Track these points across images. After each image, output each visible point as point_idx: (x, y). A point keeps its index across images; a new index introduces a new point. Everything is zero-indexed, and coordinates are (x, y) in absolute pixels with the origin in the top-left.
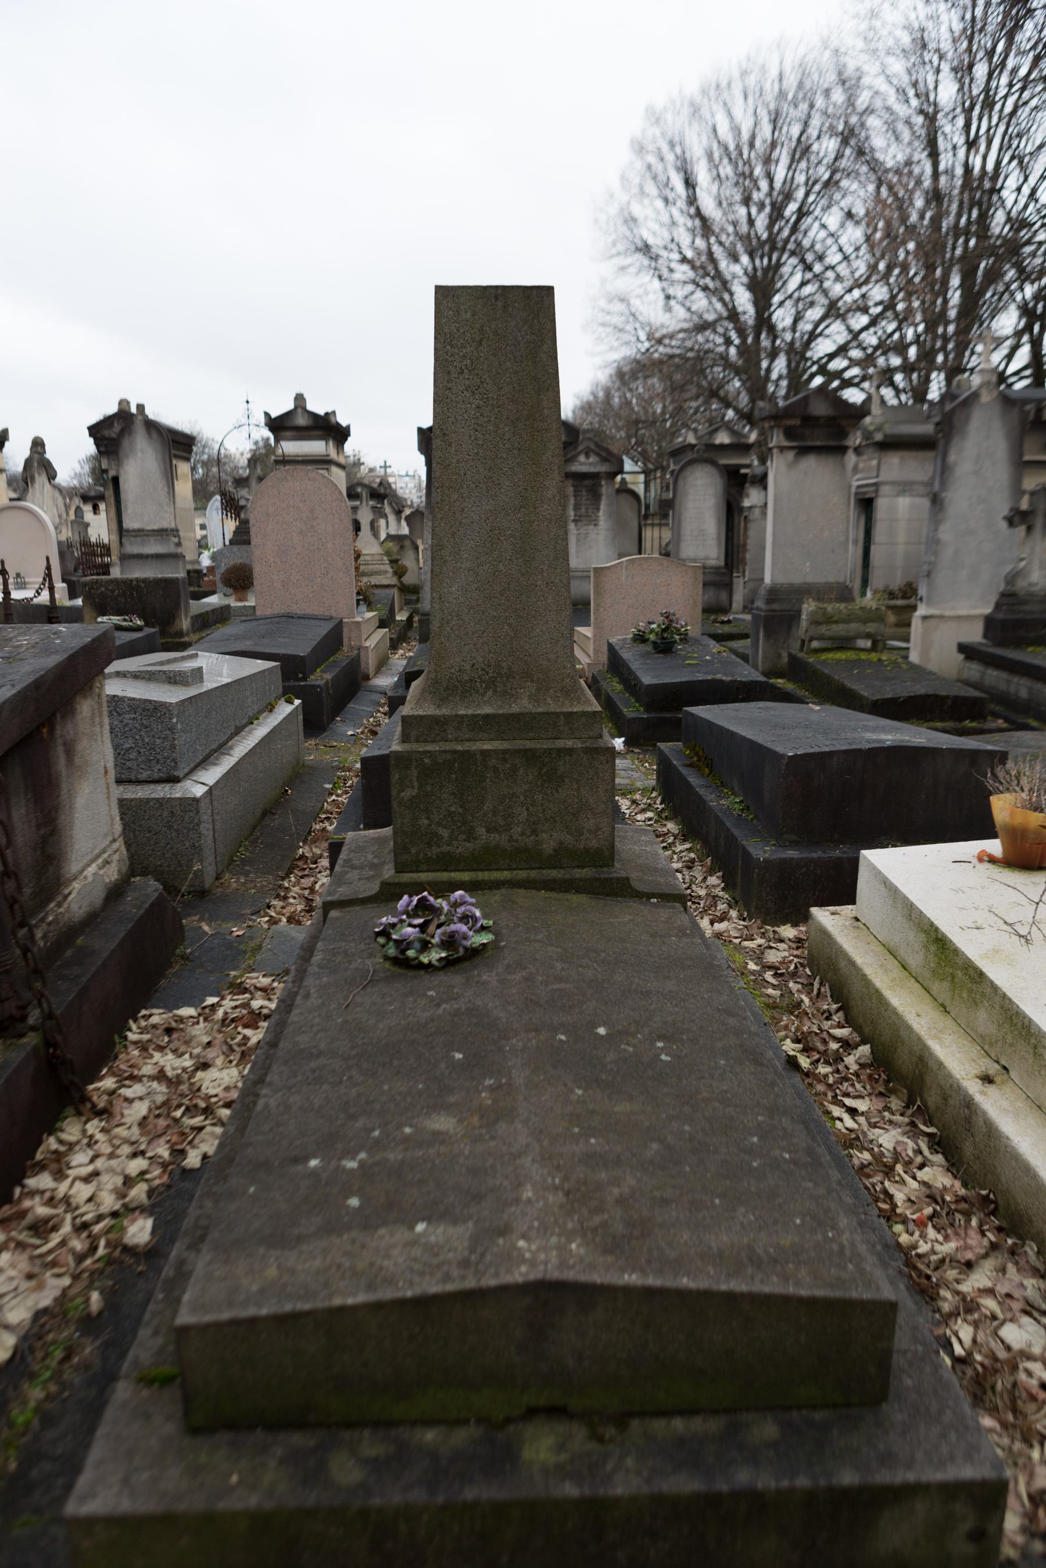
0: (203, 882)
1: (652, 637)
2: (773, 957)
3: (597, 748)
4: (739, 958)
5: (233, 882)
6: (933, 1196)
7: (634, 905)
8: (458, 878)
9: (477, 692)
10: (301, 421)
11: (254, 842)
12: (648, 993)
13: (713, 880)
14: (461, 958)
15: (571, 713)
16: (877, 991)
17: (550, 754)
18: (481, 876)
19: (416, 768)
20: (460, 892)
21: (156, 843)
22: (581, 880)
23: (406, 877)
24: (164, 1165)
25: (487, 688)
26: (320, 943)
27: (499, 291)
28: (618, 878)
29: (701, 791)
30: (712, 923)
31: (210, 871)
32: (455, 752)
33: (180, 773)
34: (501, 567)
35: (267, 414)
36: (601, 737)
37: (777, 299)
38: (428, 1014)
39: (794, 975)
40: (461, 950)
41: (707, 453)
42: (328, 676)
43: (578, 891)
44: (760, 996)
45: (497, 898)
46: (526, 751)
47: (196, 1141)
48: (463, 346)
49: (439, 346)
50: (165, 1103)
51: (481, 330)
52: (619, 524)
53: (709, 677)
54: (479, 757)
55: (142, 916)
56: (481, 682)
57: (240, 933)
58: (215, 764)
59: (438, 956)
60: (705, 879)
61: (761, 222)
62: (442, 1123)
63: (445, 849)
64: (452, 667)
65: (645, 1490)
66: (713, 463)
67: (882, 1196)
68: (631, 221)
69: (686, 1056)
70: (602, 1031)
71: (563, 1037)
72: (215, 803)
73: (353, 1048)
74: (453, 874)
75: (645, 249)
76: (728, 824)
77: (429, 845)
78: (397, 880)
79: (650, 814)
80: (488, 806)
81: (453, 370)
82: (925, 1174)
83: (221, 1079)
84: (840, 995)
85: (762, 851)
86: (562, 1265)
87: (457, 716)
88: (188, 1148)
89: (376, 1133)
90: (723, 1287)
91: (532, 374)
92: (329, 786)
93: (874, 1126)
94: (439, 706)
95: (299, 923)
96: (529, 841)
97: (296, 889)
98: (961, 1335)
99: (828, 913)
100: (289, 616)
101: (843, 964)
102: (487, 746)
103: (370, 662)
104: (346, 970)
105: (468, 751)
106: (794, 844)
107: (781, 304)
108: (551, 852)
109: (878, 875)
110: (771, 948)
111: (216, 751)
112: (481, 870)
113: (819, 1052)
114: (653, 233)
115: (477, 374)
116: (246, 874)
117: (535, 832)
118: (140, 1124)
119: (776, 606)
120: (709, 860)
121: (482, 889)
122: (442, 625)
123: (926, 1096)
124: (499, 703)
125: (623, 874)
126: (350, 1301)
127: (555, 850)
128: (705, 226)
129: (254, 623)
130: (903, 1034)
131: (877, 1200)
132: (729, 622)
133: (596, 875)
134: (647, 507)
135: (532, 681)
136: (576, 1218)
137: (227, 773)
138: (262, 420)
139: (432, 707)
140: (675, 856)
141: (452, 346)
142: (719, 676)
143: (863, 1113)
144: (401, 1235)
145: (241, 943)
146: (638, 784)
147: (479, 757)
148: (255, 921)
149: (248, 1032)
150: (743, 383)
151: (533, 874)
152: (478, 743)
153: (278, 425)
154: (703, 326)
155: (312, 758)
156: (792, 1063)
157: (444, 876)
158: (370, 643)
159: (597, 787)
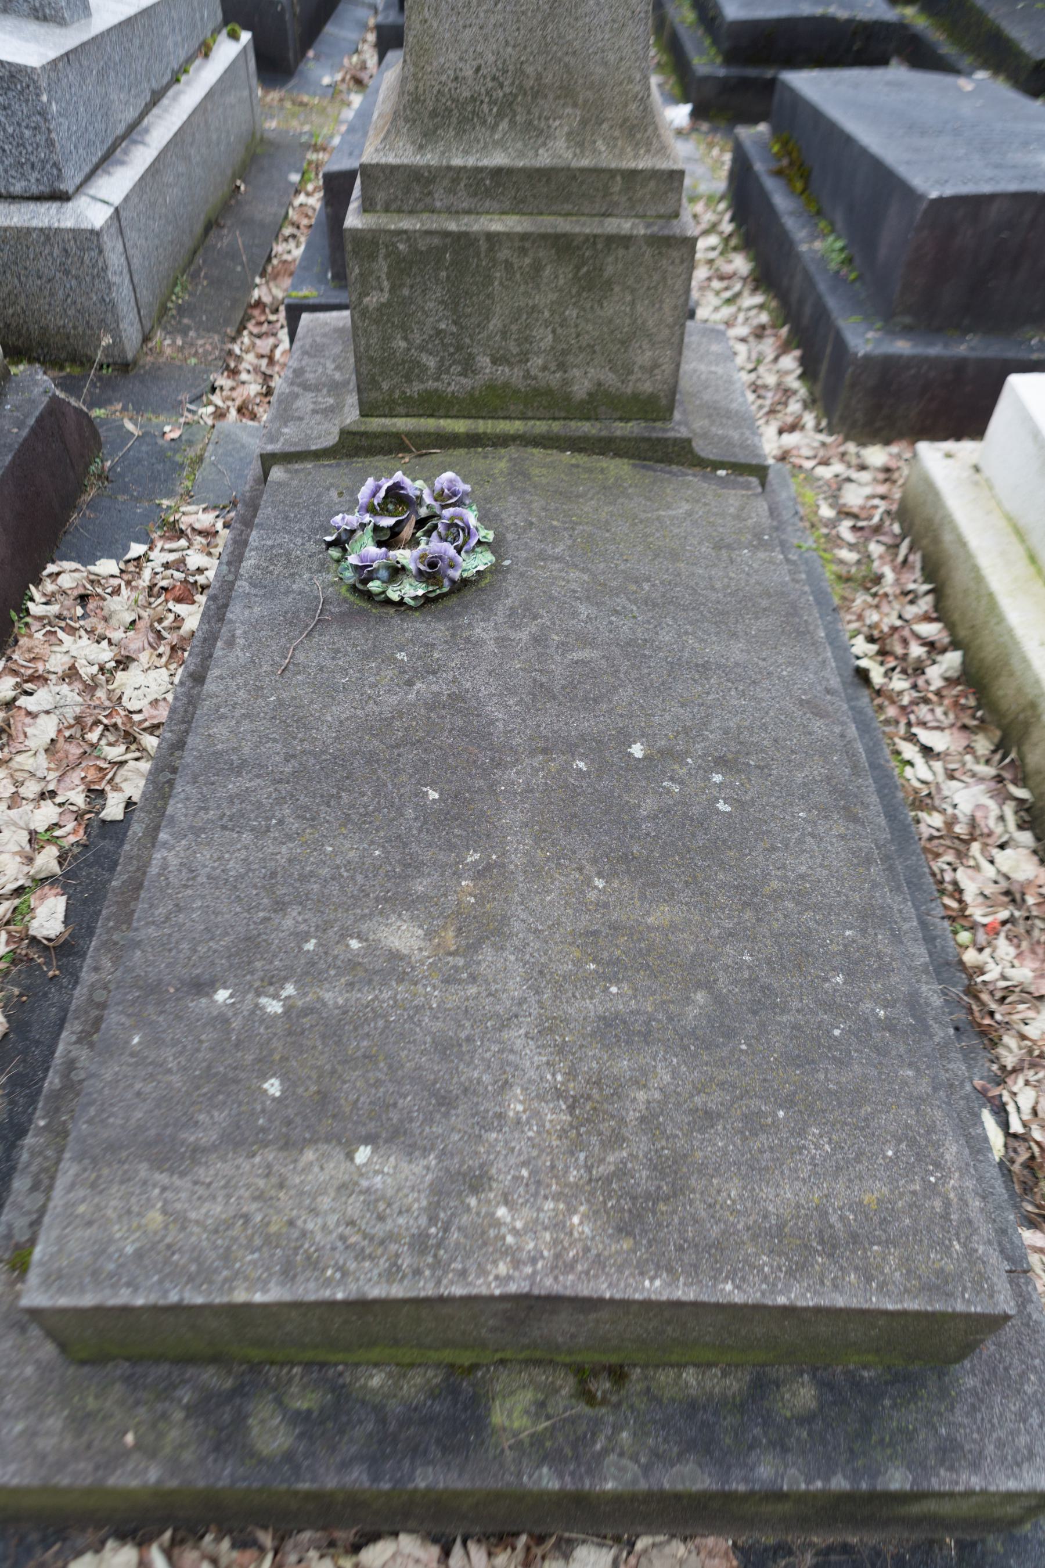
0: (123, 351)
2: (853, 497)
4: (809, 495)
5: (166, 344)
6: (1012, 896)
7: (693, 478)
8: (449, 429)
11: (195, 276)
12: (704, 668)
14: (447, 593)
16: (991, 595)
17: (595, 243)
18: (483, 426)
20: (449, 475)
21: (52, 295)
22: (623, 439)
23: (376, 424)
24: (79, 816)
25: (500, 116)
26: (254, 533)
28: (675, 440)
29: (790, 223)
30: (781, 432)
31: (131, 332)
32: (447, 234)
33: (68, 186)
36: (676, 215)
38: (394, 700)
39: (877, 530)
40: (446, 582)
43: (617, 454)
44: (832, 561)
45: (503, 465)
47: (117, 780)
50: (78, 719)
54: (483, 245)
55: (26, 440)
56: (490, 103)
57: (175, 435)
58: (122, 163)
59: (413, 593)
60: (776, 359)
62: (403, 936)
63: (431, 385)
64: (442, 70)
65: (643, 1485)
67: (950, 888)
69: (753, 800)
70: (637, 750)
71: (581, 765)
72: (127, 232)
73: (288, 758)
74: (442, 422)
76: (822, 287)
78: (363, 428)
80: (495, 323)
82: (1006, 859)
83: (148, 686)
84: (935, 572)
85: (864, 339)
86: (560, 1265)
87: (449, 168)
88: (108, 788)
89: (310, 946)
90: (781, 1300)
93: (951, 776)
94: (421, 147)
95: (254, 417)
96: (555, 379)
97: (250, 357)
98: (1020, 1099)
99: (939, 455)
101: (947, 538)
102: (497, 225)
104: (287, 593)
105: (466, 234)
106: (907, 331)
108: (585, 396)
109: (1026, 419)
110: (849, 480)
111: (123, 138)
112: (483, 418)
113: (896, 658)
116: (184, 331)
117: (562, 366)
118: (46, 751)
120: (784, 331)
121: (484, 446)
123: (1026, 748)
124: (519, 145)
125: (683, 432)
126: (258, 1298)
130: (1015, 661)
131: (942, 892)
133: (645, 432)
135: (575, 105)
136: (582, 1156)
137: (142, 178)
139: (410, 149)
143: (938, 754)
144: (335, 1169)
145: (176, 451)
147: (483, 245)
148: (194, 412)
149: (181, 609)
151: (556, 427)
156: (863, 676)
157: (429, 424)
159: (661, 302)
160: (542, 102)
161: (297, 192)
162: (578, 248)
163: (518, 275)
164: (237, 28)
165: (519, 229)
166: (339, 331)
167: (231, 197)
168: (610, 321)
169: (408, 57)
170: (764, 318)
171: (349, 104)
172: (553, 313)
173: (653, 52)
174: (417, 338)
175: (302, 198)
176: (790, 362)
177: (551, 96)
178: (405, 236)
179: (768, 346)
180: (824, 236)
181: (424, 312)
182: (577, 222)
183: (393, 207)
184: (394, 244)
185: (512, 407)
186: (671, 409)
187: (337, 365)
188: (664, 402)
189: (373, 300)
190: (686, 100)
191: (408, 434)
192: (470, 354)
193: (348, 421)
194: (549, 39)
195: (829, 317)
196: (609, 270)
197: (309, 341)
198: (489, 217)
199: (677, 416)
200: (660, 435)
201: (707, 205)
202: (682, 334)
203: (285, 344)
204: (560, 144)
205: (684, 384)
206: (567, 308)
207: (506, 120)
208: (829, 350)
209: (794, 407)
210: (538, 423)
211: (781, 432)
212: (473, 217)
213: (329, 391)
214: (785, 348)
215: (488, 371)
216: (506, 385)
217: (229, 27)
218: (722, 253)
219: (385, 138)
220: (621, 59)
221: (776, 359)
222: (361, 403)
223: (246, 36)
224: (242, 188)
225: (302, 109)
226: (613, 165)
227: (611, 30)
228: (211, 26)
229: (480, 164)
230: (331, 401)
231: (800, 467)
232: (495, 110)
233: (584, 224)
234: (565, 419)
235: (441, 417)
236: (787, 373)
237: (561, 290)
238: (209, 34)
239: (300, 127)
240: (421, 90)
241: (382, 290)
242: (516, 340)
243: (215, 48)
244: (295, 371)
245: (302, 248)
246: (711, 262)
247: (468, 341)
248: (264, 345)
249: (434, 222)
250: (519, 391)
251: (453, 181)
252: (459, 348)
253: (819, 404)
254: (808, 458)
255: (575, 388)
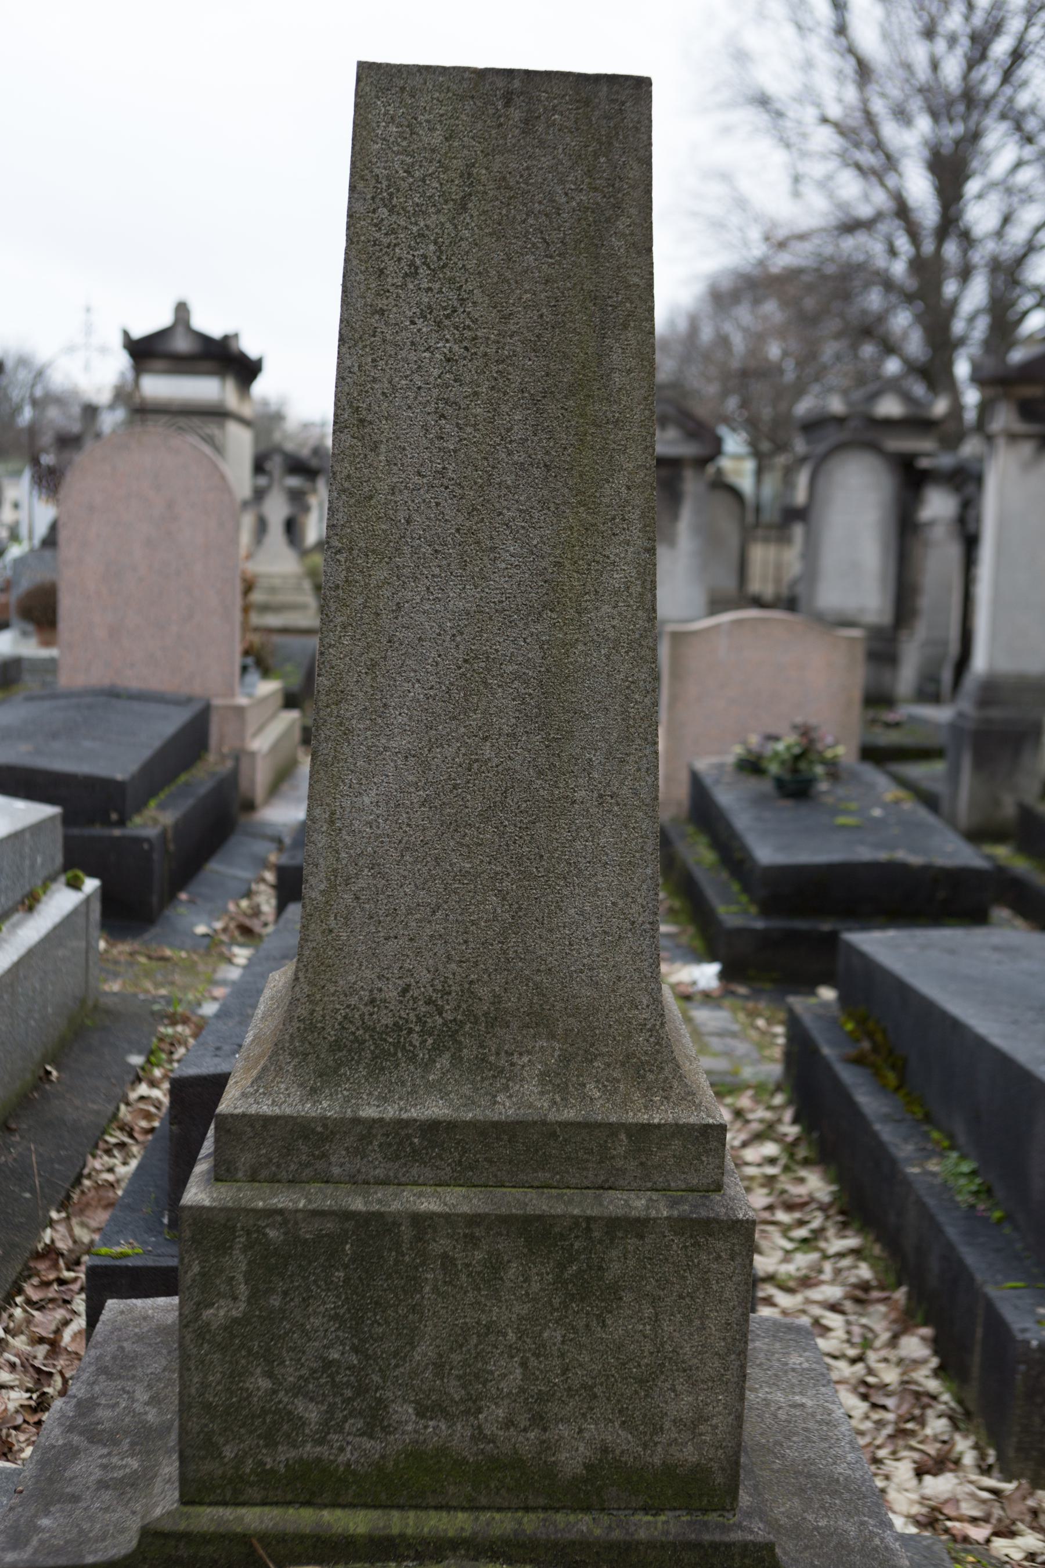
1: (774, 768)
3: (707, 1222)
8: (338, 1528)
9: (412, 1059)
10: (182, 344)
13: (914, 1345)
15: (647, 1128)
17: (588, 1229)
19: (244, 1250)
22: (651, 1545)
25: (438, 1049)
27: (517, 84)
28: (745, 1545)
29: (886, 1132)
30: (920, 1473)
32: (348, 1215)
34: (487, 751)
35: (126, 334)
36: (719, 1187)
37: (972, 187)
41: (863, 432)
42: (168, 818)
46: (527, 1220)
48: (420, 211)
49: (360, 207)
51: (467, 175)
52: (709, 539)
53: (883, 856)
54: (406, 1232)
61: (952, 70)
63: (310, 1450)
64: (353, 991)
66: (873, 447)
68: (741, 57)
74: (326, 1515)
75: (763, 101)
76: (952, 1232)
77: (270, 1440)
78: (182, 1526)
79: (770, 1149)
80: (424, 1351)
81: (391, 267)
87: (356, 1121)
91: (588, 286)
92: (136, 1060)
94: (314, 1091)
96: (526, 1442)
100: (113, 693)
102: (429, 1204)
103: (261, 776)
105: (380, 1216)
107: (980, 196)
108: (580, 1470)
112: (400, 1507)
114: (776, 77)
115: (452, 280)
117: (539, 1420)
119: (995, 713)
120: (900, 1295)
122: (333, 887)
124: (466, 1089)
125: (758, 1531)
127: (586, 1466)
128: (864, 72)
129: (47, 704)
132: (897, 725)
134: (758, 509)
135: (552, 1036)
138: (116, 342)
139: (296, 1093)
140: (828, 1267)
141: (391, 211)
142: (901, 855)
146: (747, 1073)
147: (406, 1232)
150: (919, 318)
151: (531, 1523)
152: (407, 1193)
153: (145, 352)
154: (851, 226)
155: (115, 986)
158: (261, 743)
159: (703, 1317)
160: (500, 1031)
161: (139, 1080)
162: (563, 1237)
163: (464, 1278)
164: (80, 874)
165: (465, 1209)
166: (161, 1330)
167: (36, 1088)
168: (620, 1347)
169: (301, 975)
170: (865, 1272)
171: (229, 961)
172: (521, 1334)
173: (662, 895)
174: (290, 1374)
175: (143, 1089)
176: (914, 1345)
177: (515, 1025)
178: (279, 1218)
179: (878, 1320)
180: (942, 1155)
181: (305, 1333)
182: (560, 1197)
183: (264, 1174)
184: (260, 1230)
185: (451, 1489)
186: (732, 1491)
187: (148, 1400)
188: (720, 1479)
189: (218, 1314)
190: (712, 958)
191: (264, 1538)
192: (380, 1401)
193: (158, 1512)
194: (511, 955)
195: (971, 1279)
196: (615, 1269)
197: (111, 1348)
198: (416, 1189)
199: (744, 1499)
200: (717, 1537)
201: (756, 1099)
202: (743, 1367)
203: (80, 1323)
204: (531, 1088)
205: (751, 1430)
206: (546, 1326)
207: (447, 1055)
208: (979, 1333)
209: (937, 1425)
210: (498, 1516)
211: (920, 1473)
212: (391, 1189)
213: (133, 1444)
214: (904, 1325)
215: (409, 1428)
216: (442, 1451)
217: (70, 874)
218: (786, 1169)
219: (259, 1078)
220: (619, 978)
221: (893, 1342)
222: (184, 1480)
223: (91, 884)
224: (55, 1073)
225: (161, 963)
226: (613, 1119)
227: (603, 943)
228: (43, 873)
229: (405, 1116)
230: (134, 1464)
231: (966, 1539)
232: (430, 1041)
233: (570, 1202)
234: (545, 1509)
235: (325, 1506)
236: (917, 1363)
237: (535, 1300)
238: (39, 882)
239: (154, 990)
240: (318, 1016)
241: (235, 1299)
242: (459, 1378)
243: (44, 899)
244: (79, 1404)
245: (134, 1163)
246: (770, 1181)
247: (376, 1378)
248: (45, 1322)
249: (327, 1198)
250: (465, 1461)
251: (361, 1138)
252: (361, 1390)
253: (978, 1420)
254: (974, 1520)
255: (563, 1456)
